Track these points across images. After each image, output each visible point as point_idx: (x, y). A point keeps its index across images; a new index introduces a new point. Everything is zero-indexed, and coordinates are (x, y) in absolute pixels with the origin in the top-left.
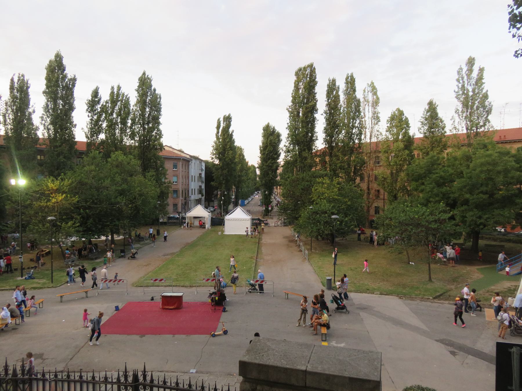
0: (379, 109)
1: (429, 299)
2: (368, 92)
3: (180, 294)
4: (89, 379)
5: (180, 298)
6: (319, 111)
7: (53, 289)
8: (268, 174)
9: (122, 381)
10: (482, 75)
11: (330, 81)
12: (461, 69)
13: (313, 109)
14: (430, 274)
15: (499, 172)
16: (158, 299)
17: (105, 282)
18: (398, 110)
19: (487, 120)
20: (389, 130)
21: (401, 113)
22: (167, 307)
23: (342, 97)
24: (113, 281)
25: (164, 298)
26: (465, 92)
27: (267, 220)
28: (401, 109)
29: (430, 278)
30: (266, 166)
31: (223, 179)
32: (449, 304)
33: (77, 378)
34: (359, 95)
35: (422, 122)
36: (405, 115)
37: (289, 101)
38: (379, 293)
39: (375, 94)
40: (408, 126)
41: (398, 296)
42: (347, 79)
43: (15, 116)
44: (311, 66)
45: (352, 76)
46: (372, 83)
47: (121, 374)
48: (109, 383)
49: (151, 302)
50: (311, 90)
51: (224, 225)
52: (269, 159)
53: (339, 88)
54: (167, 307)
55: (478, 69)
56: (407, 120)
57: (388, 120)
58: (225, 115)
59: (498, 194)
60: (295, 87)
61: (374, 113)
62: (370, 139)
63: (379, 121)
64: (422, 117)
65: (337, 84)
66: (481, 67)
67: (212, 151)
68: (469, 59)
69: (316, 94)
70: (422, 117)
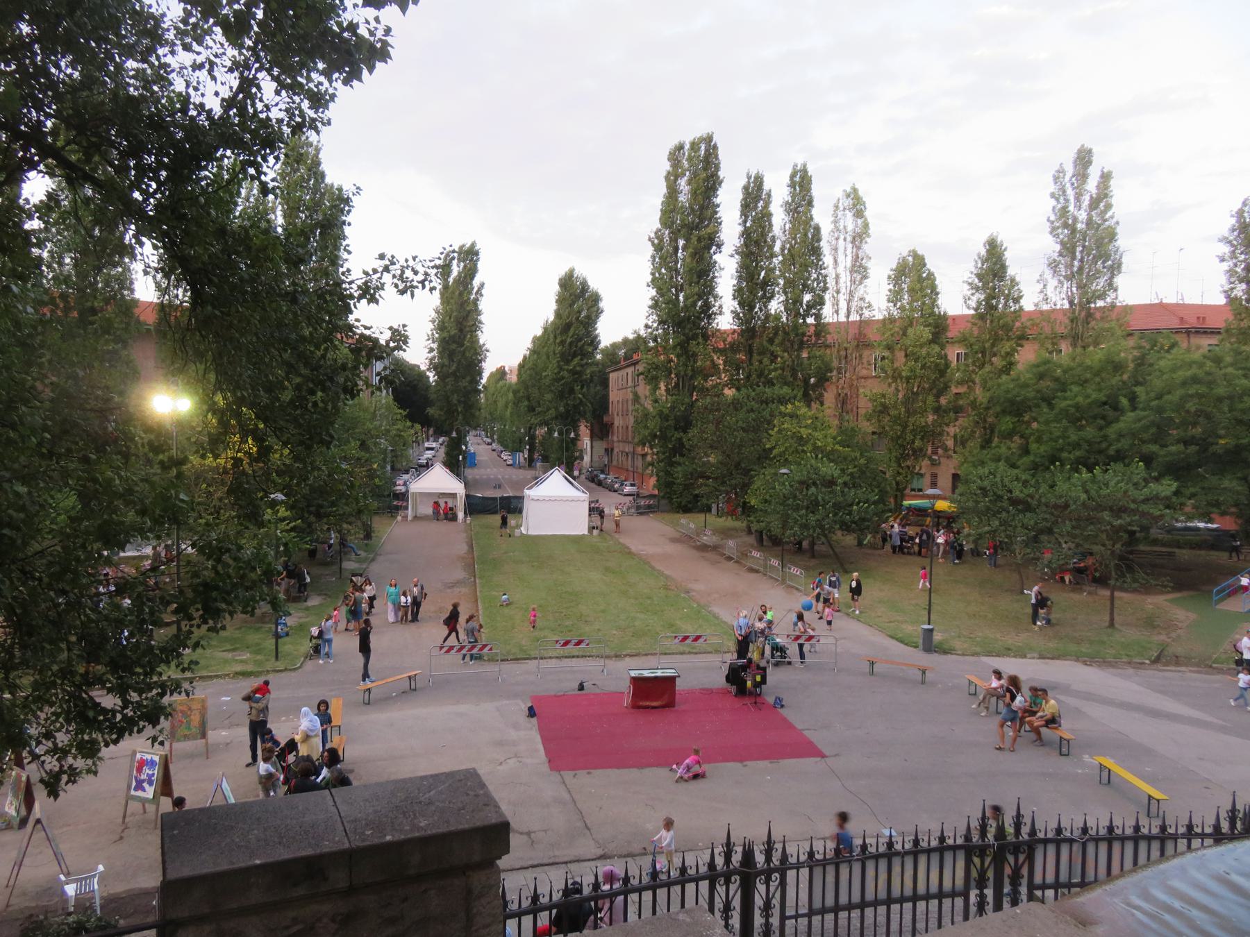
0: (869, 247)
1: (1144, 663)
2: (844, 209)
3: (669, 673)
4: (908, 846)
5: (671, 681)
6: (724, 248)
7: (288, 674)
8: (572, 391)
9: (1224, 831)
10: (1107, 187)
11: (749, 177)
12: (1061, 171)
13: (710, 241)
14: (1112, 614)
15: (1220, 399)
16: (625, 687)
17: (448, 651)
18: (915, 254)
19: (1110, 285)
20: (895, 297)
21: (919, 261)
22: (648, 703)
23: (779, 220)
24: (455, 649)
25: (636, 681)
26: (1070, 222)
27: (597, 501)
28: (920, 252)
29: (1112, 620)
30: (567, 370)
31: (459, 401)
32: (1191, 671)
33: (1155, 831)
34: (821, 215)
35: (970, 284)
36: (928, 266)
37: (652, 222)
38: (1036, 655)
39: (859, 214)
40: (934, 292)
41: (1077, 660)
42: (792, 176)
43: (164, 247)
44: (709, 139)
45: (804, 170)
46: (855, 190)
47: (1223, 815)
48: (1197, 835)
49: (579, 695)
50: (709, 198)
51: (520, 511)
52: (574, 355)
53: (769, 195)
54: (648, 703)
55: (1099, 174)
56: (931, 276)
57: (889, 277)
58: (463, 246)
59: (1217, 444)
60: (668, 187)
61: (856, 258)
62: (848, 317)
63: (865, 277)
64: (972, 273)
65: (766, 187)
66: (1105, 170)
67: (430, 333)
68: (1080, 152)
69: (718, 206)
70: (972, 273)
